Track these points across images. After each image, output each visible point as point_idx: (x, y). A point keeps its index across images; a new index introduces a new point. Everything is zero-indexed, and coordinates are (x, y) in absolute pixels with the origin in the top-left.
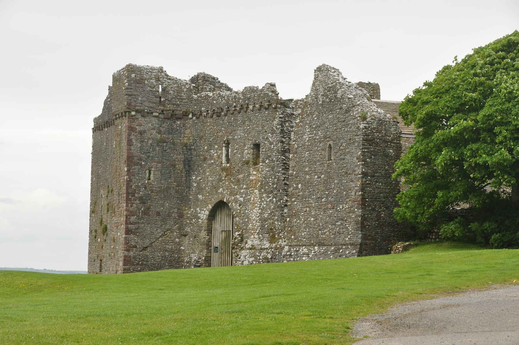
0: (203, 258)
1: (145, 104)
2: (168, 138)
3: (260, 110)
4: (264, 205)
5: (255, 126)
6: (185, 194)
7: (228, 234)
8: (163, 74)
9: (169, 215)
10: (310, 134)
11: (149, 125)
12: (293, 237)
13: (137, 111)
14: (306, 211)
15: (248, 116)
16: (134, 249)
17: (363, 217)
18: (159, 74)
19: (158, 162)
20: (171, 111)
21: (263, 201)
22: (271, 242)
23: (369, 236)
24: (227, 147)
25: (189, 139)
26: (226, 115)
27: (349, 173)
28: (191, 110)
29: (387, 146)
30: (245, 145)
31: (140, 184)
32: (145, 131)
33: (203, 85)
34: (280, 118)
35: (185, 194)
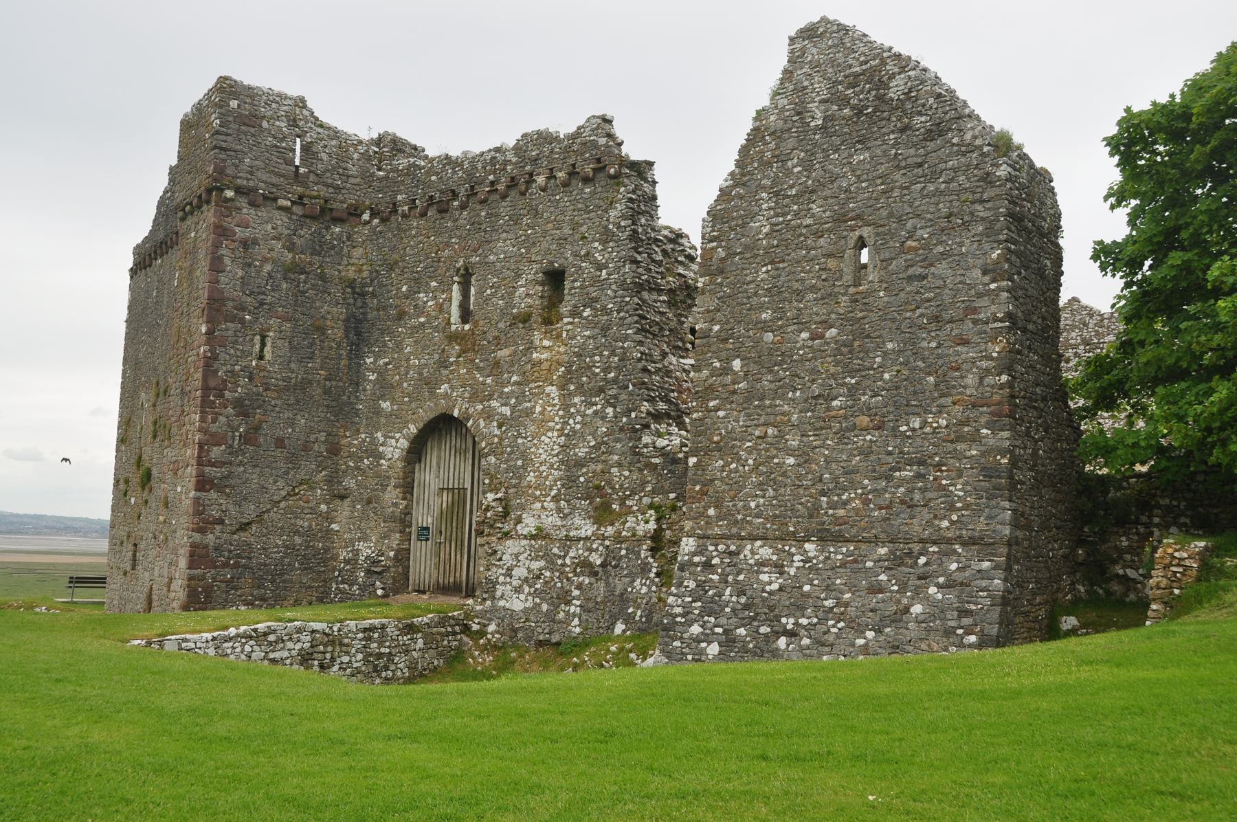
1: (259, 174)
2: (310, 264)
3: (566, 184)
4: (575, 423)
5: (550, 226)
6: (345, 398)
9: (306, 448)
10: (777, 215)
11: (267, 227)
12: (711, 512)
13: (239, 190)
16: (218, 527)
19: (285, 319)
20: (322, 202)
21: (572, 416)
22: (598, 522)
25: (360, 271)
26: (463, 207)
28: (367, 203)
30: (518, 276)
31: (237, 368)
32: (255, 242)
34: (631, 200)
35: (345, 398)
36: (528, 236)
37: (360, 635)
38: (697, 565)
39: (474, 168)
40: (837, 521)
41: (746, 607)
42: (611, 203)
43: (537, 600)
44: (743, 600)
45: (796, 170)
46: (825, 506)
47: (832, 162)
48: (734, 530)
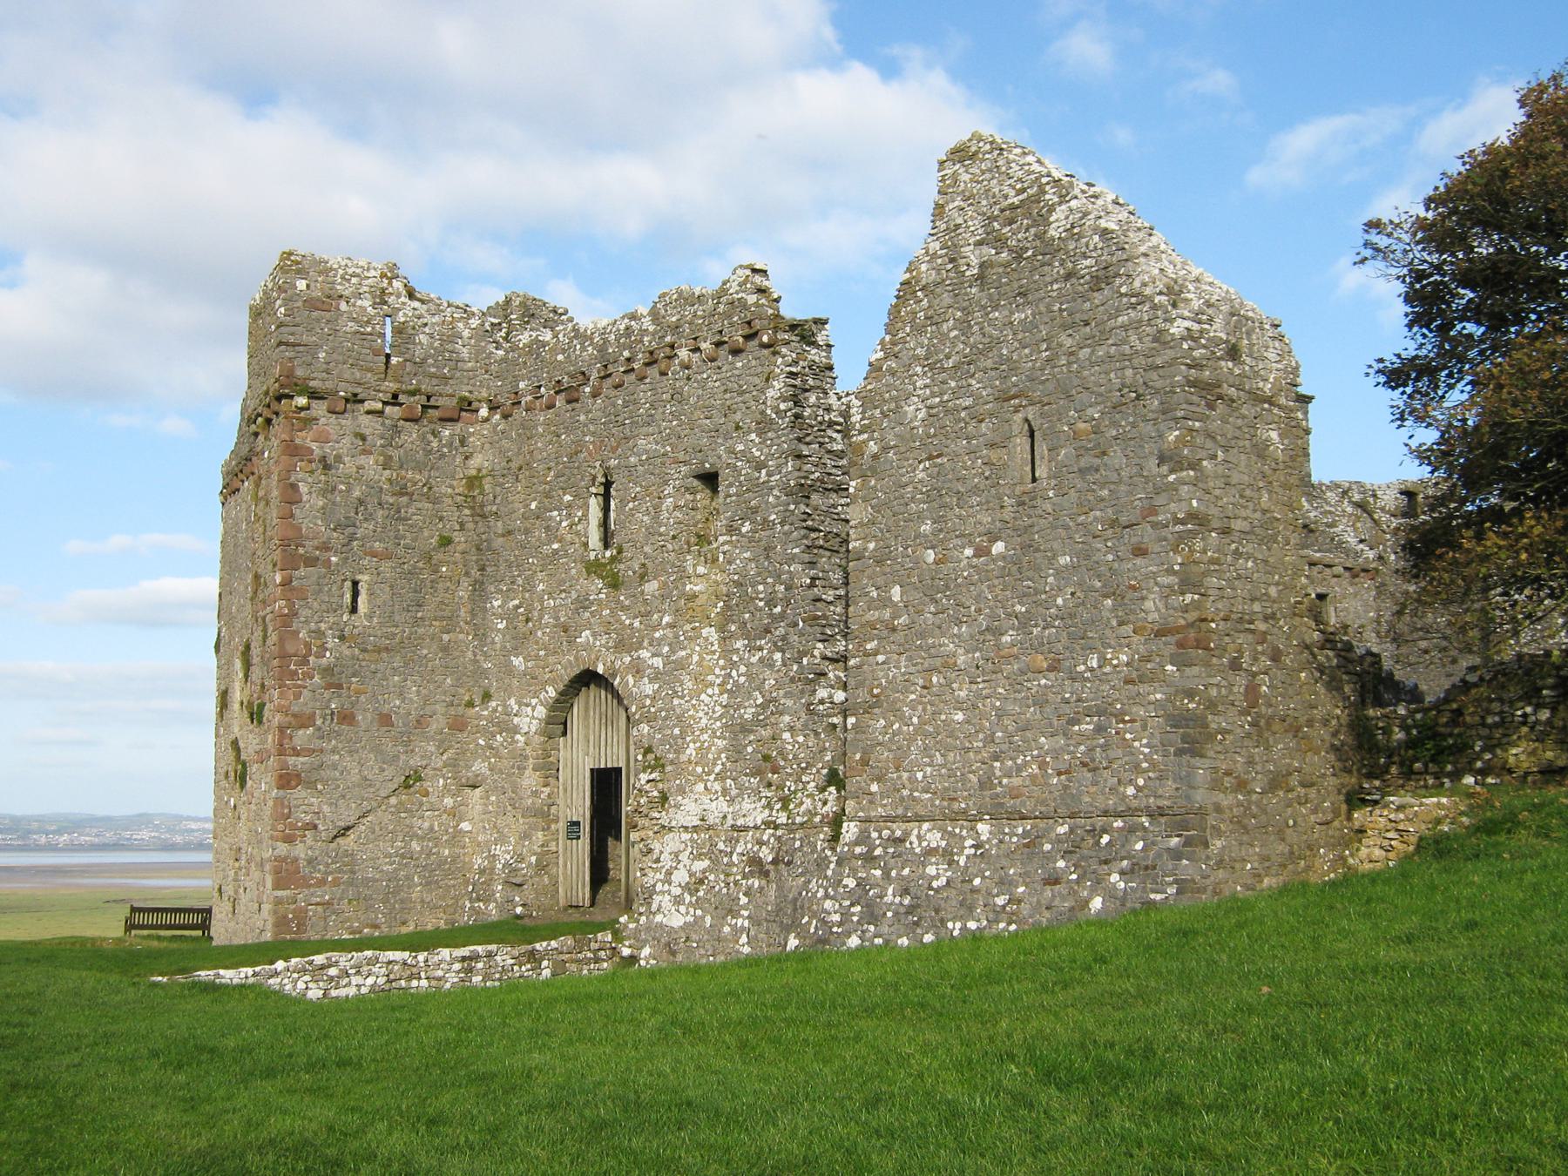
0: (533, 859)
10: (933, 395)
21: (734, 665)
23: (1228, 773)
26: (595, 395)
34: (792, 375)
37: (457, 966)
38: (857, 857)
39: (606, 341)
40: (1014, 793)
41: (910, 910)
42: (767, 380)
43: (699, 912)
44: (906, 901)
45: (953, 334)
46: (998, 773)
47: (991, 322)
48: (900, 811)
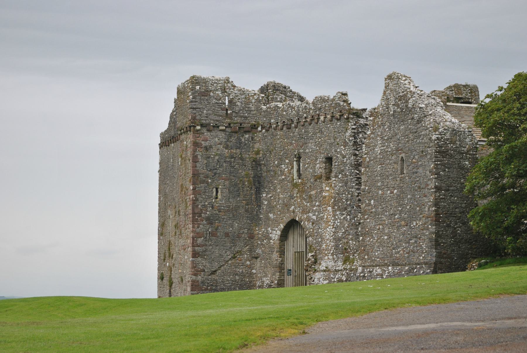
0: (276, 282)
1: (210, 117)
3: (331, 121)
7: (300, 256)
8: (229, 85)
9: (239, 237)
10: (382, 146)
11: (216, 139)
12: (366, 257)
13: (202, 125)
14: (379, 229)
15: (319, 128)
16: (202, 273)
17: (437, 234)
18: (226, 86)
21: (336, 220)
23: (445, 254)
24: (298, 161)
26: (296, 127)
27: (422, 187)
29: (462, 158)
30: (317, 159)
31: (206, 203)
32: (211, 147)
33: (273, 95)
34: (353, 129)
35: (255, 212)
36: (319, 142)
39: (299, 110)
48: (372, 263)
